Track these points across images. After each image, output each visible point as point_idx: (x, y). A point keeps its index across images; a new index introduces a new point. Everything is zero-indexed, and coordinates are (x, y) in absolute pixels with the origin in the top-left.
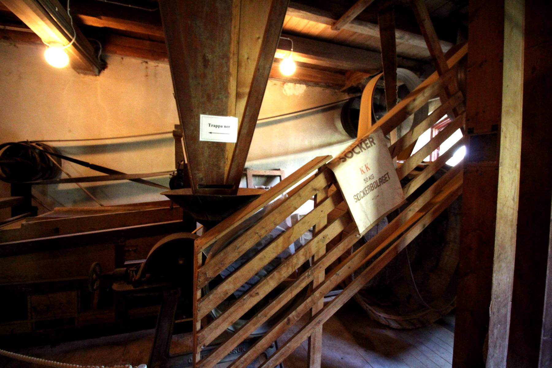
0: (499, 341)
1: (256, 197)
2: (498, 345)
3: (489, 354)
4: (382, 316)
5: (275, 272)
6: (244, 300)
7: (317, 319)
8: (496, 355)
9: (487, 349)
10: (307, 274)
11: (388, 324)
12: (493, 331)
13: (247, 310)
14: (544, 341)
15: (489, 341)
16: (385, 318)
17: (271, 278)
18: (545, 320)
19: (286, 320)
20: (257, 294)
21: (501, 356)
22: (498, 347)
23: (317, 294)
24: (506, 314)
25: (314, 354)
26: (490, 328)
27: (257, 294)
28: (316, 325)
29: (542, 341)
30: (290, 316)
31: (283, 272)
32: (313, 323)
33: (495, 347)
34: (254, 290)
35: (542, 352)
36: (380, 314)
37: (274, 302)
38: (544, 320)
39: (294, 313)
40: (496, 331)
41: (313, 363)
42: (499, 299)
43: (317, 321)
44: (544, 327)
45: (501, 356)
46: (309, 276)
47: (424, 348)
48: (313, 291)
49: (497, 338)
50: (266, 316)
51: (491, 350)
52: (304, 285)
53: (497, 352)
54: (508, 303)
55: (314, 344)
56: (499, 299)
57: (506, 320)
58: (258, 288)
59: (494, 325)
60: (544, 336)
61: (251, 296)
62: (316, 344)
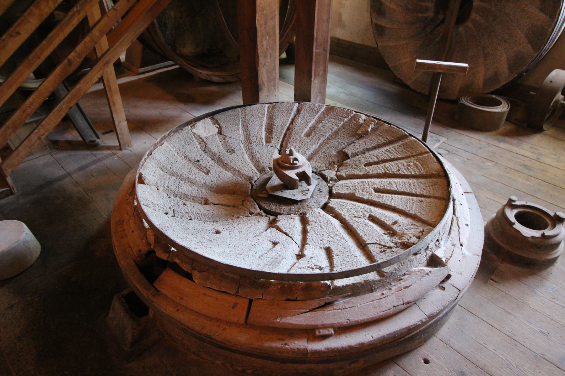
0: (270, 51)
1: (109, 219)
2: (269, 56)
3: (260, 62)
4: (204, 73)
5: (32, 7)
6: (4, 40)
7: (104, 60)
8: (267, 64)
9: (258, 58)
10: (75, 9)
11: (209, 79)
12: (262, 42)
13: (12, 52)
14: (317, 53)
15: (259, 51)
16: (207, 75)
17: (29, 14)
18: (317, 33)
19: (66, 61)
20: (18, 33)
21: (273, 64)
22: (269, 57)
23: (95, 32)
24: (274, 28)
25: (112, 96)
26: (259, 39)
27: (18, 33)
28: (104, 65)
29: (314, 54)
30: (70, 57)
31: (42, 7)
32: (100, 64)
33: (266, 57)
34: (12, 29)
35: (315, 65)
36: (201, 71)
37: (44, 42)
38: (315, 34)
39: (73, 54)
40: (265, 42)
41: (114, 104)
42: (265, 12)
43: (105, 62)
44: (316, 41)
45: (273, 64)
46: (79, 12)
47: (507, 284)
48: (90, 30)
49: (267, 49)
50: (39, 58)
51: (261, 60)
52: (75, 22)
53: (269, 61)
54: (275, 17)
55: (109, 86)
56: (265, 12)
57: (275, 33)
58: (16, 27)
59: (263, 37)
60: (316, 49)
61: (11, 36)
62: (112, 86)
